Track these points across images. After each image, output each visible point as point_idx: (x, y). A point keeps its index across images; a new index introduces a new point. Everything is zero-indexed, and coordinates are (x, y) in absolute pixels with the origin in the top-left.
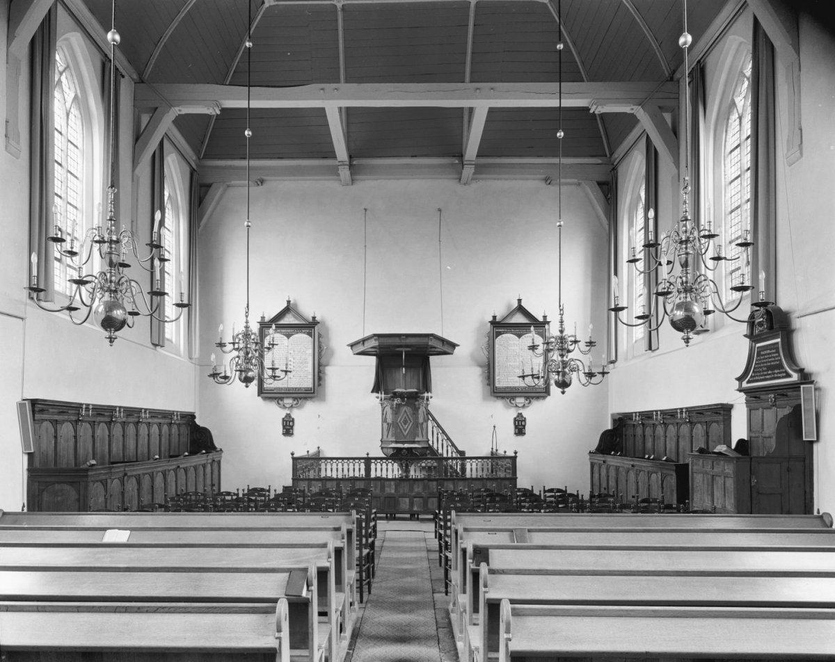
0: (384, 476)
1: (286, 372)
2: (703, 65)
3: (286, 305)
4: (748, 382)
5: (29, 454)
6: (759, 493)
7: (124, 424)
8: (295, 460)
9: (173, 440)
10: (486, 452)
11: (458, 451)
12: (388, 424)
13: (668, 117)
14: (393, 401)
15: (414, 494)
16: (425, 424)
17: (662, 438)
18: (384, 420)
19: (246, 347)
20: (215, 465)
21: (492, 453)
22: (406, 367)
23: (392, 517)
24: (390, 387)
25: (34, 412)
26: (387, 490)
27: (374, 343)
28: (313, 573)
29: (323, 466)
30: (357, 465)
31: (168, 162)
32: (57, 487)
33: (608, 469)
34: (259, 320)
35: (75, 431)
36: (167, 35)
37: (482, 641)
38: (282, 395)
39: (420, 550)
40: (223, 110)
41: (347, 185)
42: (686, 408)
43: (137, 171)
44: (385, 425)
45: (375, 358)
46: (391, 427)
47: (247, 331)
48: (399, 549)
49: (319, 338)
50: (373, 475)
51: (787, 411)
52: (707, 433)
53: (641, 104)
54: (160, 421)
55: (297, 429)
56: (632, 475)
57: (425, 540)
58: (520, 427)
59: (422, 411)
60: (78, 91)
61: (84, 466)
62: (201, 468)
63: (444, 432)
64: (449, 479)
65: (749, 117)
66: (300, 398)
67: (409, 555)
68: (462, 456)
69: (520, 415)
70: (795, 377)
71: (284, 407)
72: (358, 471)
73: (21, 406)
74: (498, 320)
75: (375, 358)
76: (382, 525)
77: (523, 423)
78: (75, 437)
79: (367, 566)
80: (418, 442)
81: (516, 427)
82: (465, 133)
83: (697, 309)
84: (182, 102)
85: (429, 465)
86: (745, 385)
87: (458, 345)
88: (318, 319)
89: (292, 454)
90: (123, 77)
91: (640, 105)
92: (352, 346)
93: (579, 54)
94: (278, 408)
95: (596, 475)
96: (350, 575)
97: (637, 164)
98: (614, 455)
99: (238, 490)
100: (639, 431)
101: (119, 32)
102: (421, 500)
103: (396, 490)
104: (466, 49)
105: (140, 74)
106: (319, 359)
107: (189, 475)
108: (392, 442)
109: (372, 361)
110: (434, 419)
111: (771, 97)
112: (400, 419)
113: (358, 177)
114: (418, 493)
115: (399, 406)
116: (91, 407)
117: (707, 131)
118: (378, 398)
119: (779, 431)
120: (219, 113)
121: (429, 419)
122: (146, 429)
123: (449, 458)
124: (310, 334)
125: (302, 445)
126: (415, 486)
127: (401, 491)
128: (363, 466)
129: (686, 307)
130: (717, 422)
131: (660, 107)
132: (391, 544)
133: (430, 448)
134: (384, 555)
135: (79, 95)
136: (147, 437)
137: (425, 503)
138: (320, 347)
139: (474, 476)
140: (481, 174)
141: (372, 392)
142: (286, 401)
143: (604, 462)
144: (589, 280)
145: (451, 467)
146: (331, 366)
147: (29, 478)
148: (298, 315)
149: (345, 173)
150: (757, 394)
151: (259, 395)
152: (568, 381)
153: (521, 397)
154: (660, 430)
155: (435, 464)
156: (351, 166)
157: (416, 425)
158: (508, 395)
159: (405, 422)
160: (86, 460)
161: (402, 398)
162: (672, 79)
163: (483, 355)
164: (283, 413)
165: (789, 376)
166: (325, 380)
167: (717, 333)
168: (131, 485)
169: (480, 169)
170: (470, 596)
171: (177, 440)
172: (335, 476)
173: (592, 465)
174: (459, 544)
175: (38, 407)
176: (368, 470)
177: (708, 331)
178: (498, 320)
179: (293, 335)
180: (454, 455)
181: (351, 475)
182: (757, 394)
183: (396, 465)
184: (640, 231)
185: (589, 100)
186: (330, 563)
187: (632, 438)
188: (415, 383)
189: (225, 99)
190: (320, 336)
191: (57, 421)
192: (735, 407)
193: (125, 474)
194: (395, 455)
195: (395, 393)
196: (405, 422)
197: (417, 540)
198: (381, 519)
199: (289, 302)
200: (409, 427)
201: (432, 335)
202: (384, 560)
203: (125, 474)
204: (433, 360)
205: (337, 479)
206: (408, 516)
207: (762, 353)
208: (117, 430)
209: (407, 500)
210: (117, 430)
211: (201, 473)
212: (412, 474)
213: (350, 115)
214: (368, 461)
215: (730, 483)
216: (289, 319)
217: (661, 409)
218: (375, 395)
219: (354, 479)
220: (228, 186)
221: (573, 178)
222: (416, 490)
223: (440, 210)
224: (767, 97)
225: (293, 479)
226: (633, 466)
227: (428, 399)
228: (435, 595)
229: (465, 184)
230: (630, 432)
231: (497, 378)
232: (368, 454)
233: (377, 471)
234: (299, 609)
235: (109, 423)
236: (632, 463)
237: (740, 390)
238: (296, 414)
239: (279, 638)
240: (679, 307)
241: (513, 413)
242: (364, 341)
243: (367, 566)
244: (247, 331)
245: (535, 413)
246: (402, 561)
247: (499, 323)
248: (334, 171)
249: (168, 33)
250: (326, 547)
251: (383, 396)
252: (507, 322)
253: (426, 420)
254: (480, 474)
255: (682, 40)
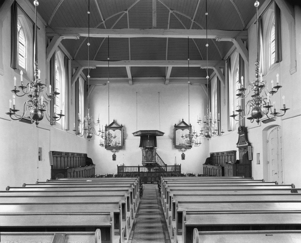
2: (262, 19)
3: (113, 121)
4: (239, 145)
7: (71, 157)
8: (118, 167)
10: (173, 164)
11: (165, 164)
13: (222, 70)
16: (155, 157)
17: (222, 160)
18: (143, 155)
19: (109, 137)
20: (94, 169)
23: (146, 183)
25: (53, 154)
26: (144, 175)
27: (140, 133)
28: (112, 215)
29: (125, 169)
30: (136, 168)
31: (57, 54)
32: (59, 174)
34: (105, 126)
36: (57, 8)
38: (112, 148)
40: (97, 67)
41: (131, 85)
43: (72, 85)
44: (143, 157)
45: (140, 137)
46: (145, 157)
47: (109, 133)
50: (140, 171)
51: (246, 153)
54: (78, 156)
55: (117, 158)
58: (183, 157)
59: (154, 152)
63: (161, 159)
65: (238, 76)
68: (166, 166)
69: (183, 153)
70: (247, 144)
71: (113, 152)
72: (136, 170)
73: (50, 153)
74: (176, 125)
75: (140, 137)
76: (143, 185)
81: (182, 157)
84: (87, 65)
85: (156, 168)
86: (238, 146)
87: (164, 133)
88: (123, 125)
89: (117, 165)
90: (69, 59)
91: (234, 38)
92: (133, 134)
93: (199, 48)
94: (111, 152)
95: (205, 171)
96: (138, 193)
97: (236, 57)
98: (209, 165)
99: (105, 175)
100: (216, 157)
101: (90, 75)
102: (154, 178)
104: (166, 46)
105: (73, 58)
107: (88, 172)
108: (145, 162)
109: (139, 138)
110: (158, 155)
112: (148, 155)
113: (134, 83)
115: (147, 151)
116: (64, 153)
117: (231, 76)
120: (79, 38)
121: (156, 155)
122: (56, 159)
123: (162, 166)
124: (120, 130)
125: (120, 161)
126: (152, 174)
127: (148, 175)
128: (137, 169)
129: (208, 133)
130: (233, 155)
131: (219, 67)
132: (146, 189)
133: (157, 163)
135: (59, 66)
136: (60, 162)
137: (155, 179)
138: (123, 134)
139: (169, 171)
140: (171, 82)
141: (139, 147)
142: (114, 150)
143: (206, 167)
144: (203, 113)
145: (163, 169)
148: (117, 124)
149: (131, 82)
152: (191, 145)
154: (221, 157)
155: (158, 168)
156: (132, 80)
157: (152, 157)
158: (179, 147)
159: (149, 156)
160: (66, 167)
161: (148, 149)
162: (223, 60)
163: (172, 136)
164: (113, 154)
165: (246, 144)
166: (125, 144)
169: (170, 81)
171: (82, 162)
173: (204, 168)
175: (54, 153)
176: (139, 170)
177: (231, 130)
178: (176, 125)
180: (164, 165)
183: (147, 169)
185: (200, 65)
186: (125, 201)
187: (215, 160)
188: (152, 144)
190: (123, 130)
191: (57, 157)
194: (147, 166)
195: (146, 148)
196: (149, 156)
197: (153, 188)
198: (143, 184)
199: (114, 120)
201: (157, 131)
202: (144, 191)
203: (74, 171)
204: (157, 137)
205: (130, 172)
206: (150, 183)
209: (150, 178)
210: (69, 158)
212: (151, 171)
213: (132, 68)
214: (139, 167)
215: (232, 170)
216: (114, 125)
218: (140, 148)
219: (135, 172)
222: (153, 175)
223: (159, 92)
224: (242, 72)
226: (213, 168)
227: (156, 149)
229: (166, 85)
230: (214, 158)
232: (139, 165)
233: (142, 170)
235: (67, 157)
236: (213, 167)
238: (116, 154)
239: (120, 210)
240: (206, 133)
241: (181, 153)
242: (137, 132)
244: (109, 133)
245: (188, 153)
246: (149, 192)
247: (177, 126)
248: (127, 81)
249: (58, 7)
253: (155, 155)
254: (171, 170)
255: (255, 4)
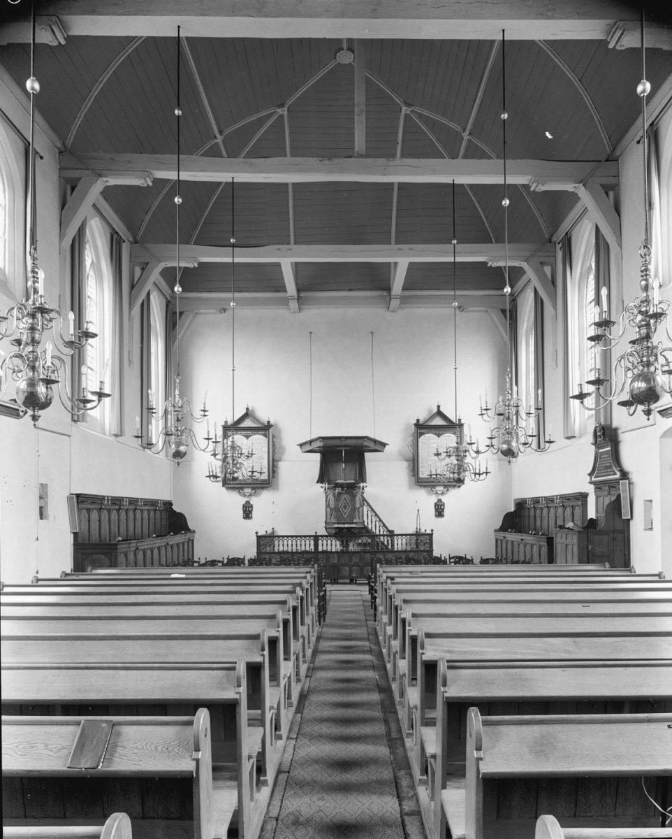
0: (329, 550)
1: (261, 473)
3: (245, 412)
4: (595, 477)
5: (74, 533)
6: (594, 556)
7: (127, 511)
8: (259, 538)
9: (157, 523)
10: (412, 530)
11: (388, 530)
12: (331, 509)
13: (548, 270)
14: (335, 490)
15: (352, 563)
16: (361, 509)
17: (547, 518)
18: (328, 506)
20: (190, 542)
21: (417, 532)
22: (345, 462)
23: (335, 582)
24: (332, 478)
25: (78, 503)
27: (319, 444)
28: (242, 669)
29: (276, 543)
30: (307, 542)
32: (95, 556)
33: (507, 543)
34: (223, 424)
35: (100, 517)
37: (474, 825)
39: (358, 600)
40: (200, 264)
42: (560, 495)
44: (328, 509)
46: (334, 511)
48: (342, 600)
49: (273, 438)
52: (573, 514)
53: (584, 182)
56: (522, 547)
57: (361, 595)
58: (439, 511)
59: (358, 498)
60: (94, 259)
61: (114, 542)
62: (176, 546)
63: (376, 515)
64: (380, 552)
66: (258, 488)
67: (350, 603)
68: (391, 534)
69: (440, 500)
70: (618, 475)
71: (245, 496)
73: (70, 498)
74: (420, 422)
77: (442, 507)
78: (99, 520)
79: (322, 609)
80: (356, 523)
81: (436, 510)
82: (392, 272)
83: (514, 444)
85: (365, 541)
86: (593, 479)
88: (272, 422)
89: (257, 533)
91: (580, 183)
92: (301, 445)
95: (499, 549)
96: (313, 610)
103: (339, 560)
105: (134, 237)
106: (273, 455)
109: (317, 456)
110: (368, 504)
111: (607, 273)
112: (341, 504)
113: (303, 307)
114: (356, 563)
115: (339, 494)
116: (110, 498)
117: (573, 286)
118: (322, 487)
119: (607, 513)
123: (381, 535)
124: (265, 435)
125: (262, 522)
128: (312, 542)
131: (541, 263)
133: (365, 528)
134: (331, 603)
138: (274, 446)
141: (317, 482)
143: (504, 537)
145: (383, 543)
146: (284, 461)
147: (74, 550)
148: (256, 420)
149: (294, 305)
150: (600, 486)
151: (223, 486)
152: (462, 478)
153: (440, 485)
154: (545, 511)
155: (369, 540)
157: (354, 509)
158: (429, 484)
159: (345, 507)
162: (550, 242)
163: (409, 452)
164: (243, 500)
167: (581, 439)
168: (140, 555)
169: (404, 300)
170: (409, 662)
172: (290, 550)
174: (407, 631)
176: (316, 545)
178: (420, 422)
179: (250, 436)
180: (385, 533)
181: (303, 549)
182: (600, 486)
184: (591, 302)
185: (529, 177)
186: (240, 693)
189: (154, 169)
190: (273, 437)
192: (590, 495)
193: (137, 548)
194: (340, 534)
195: (336, 484)
196: (345, 507)
199: (247, 409)
200: (348, 511)
204: (368, 456)
207: (602, 457)
208: (123, 514)
209: (347, 568)
210: (123, 514)
211: (181, 549)
212: (351, 548)
214: (316, 538)
215: (575, 549)
216: (248, 423)
217: (545, 495)
218: (320, 485)
220: (197, 314)
221: (481, 306)
223: (372, 333)
224: (604, 275)
225: (257, 553)
226: (522, 540)
227: (363, 489)
228: (368, 622)
229: (393, 312)
230: (526, 514)
231: (420, 470)
232: (316, 533)
234: (224, 714)
235: (118, 510)
237: (591, 483)
238: (254, 501)
241: (434, 499)
242: (311, 442)
243: (322, 609)
245: (451, 499)
247: (422, 425)
248: (285, 302)
250: (275, 618)
251: (327, 486)
252: (429, 424)
253: (362, 506)
254: (404, 548)
255: (640, 89)
